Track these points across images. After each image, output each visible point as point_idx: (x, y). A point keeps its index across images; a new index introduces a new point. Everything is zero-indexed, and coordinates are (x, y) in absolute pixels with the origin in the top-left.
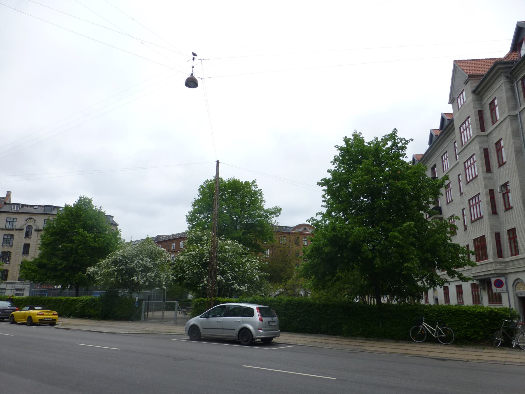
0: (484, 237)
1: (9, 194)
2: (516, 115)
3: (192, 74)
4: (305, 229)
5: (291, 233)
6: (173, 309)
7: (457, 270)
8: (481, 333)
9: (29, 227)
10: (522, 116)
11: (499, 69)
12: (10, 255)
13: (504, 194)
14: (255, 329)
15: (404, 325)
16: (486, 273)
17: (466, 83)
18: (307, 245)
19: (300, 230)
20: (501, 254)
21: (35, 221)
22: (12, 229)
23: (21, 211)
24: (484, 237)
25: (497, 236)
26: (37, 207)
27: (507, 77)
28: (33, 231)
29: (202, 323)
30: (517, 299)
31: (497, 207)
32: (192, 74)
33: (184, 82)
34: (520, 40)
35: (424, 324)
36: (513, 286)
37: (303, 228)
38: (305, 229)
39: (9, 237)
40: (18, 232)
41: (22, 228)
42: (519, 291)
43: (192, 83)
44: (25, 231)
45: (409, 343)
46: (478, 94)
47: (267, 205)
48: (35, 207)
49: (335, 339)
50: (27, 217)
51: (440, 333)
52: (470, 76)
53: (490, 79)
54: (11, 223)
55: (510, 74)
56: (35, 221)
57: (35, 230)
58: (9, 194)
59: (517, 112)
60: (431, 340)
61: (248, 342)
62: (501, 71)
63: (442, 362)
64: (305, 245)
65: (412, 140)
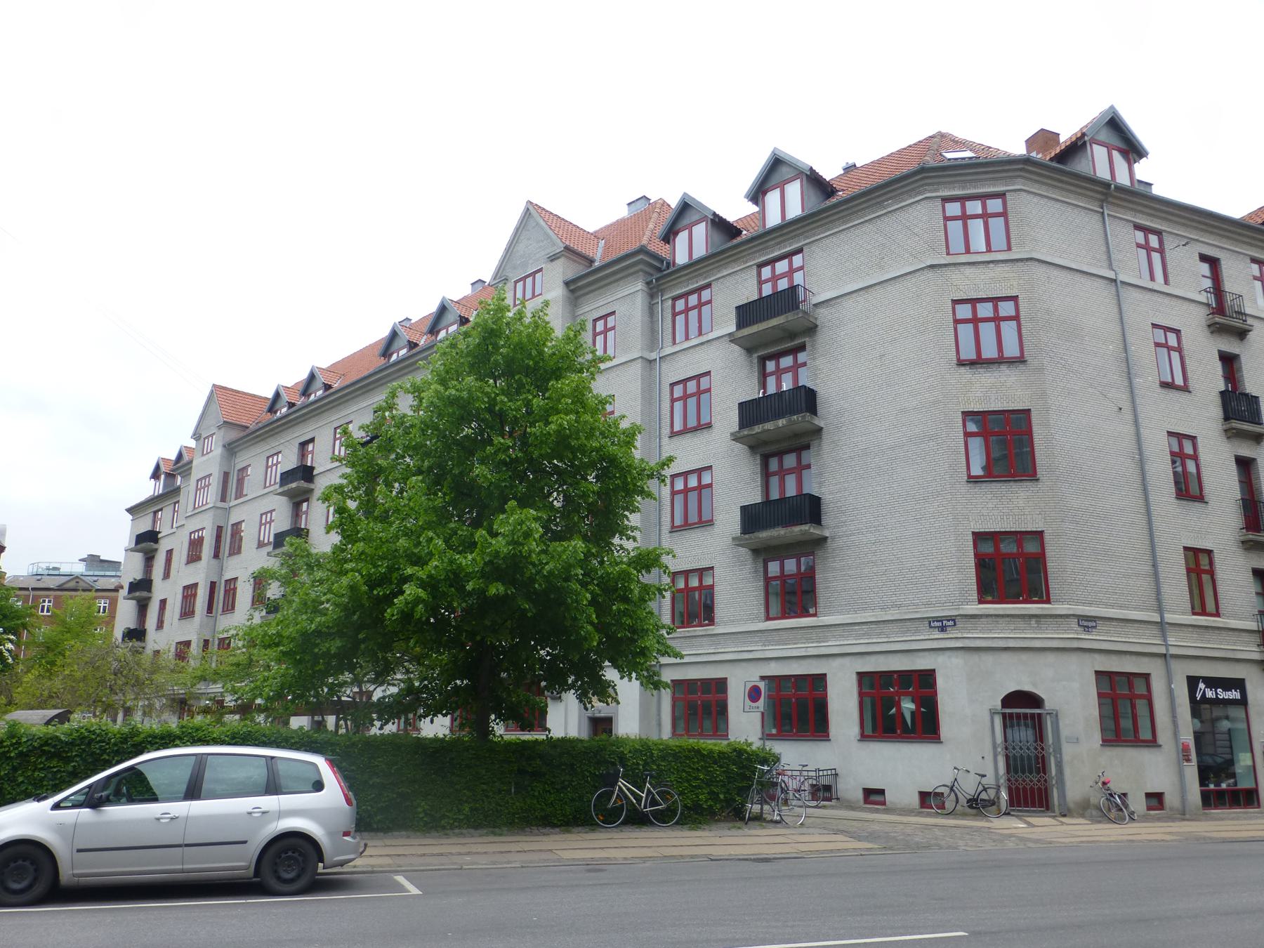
0: (196, 585)
8: (722, 796)
10: (664, 366)
11: (641, 261)
14: (331, 834)
15: (581, 791)
17: (553, 258)
24: (196, 585)
25: (213, 585)
27: (648, 283)
29: (68, 832)
34: (680, 225)
35: (621, 783)
45: (593, 830)
46: (572, 291)
49: (394, 842)
51: (654, 803)
52: (567, 248)
53: (607, 276)
54: (997, 224)
55: (657, 280)
59: (654, 356)
60: (638, 819)
61: (39, 889)
62: (641, 266)
63: (762, 866)
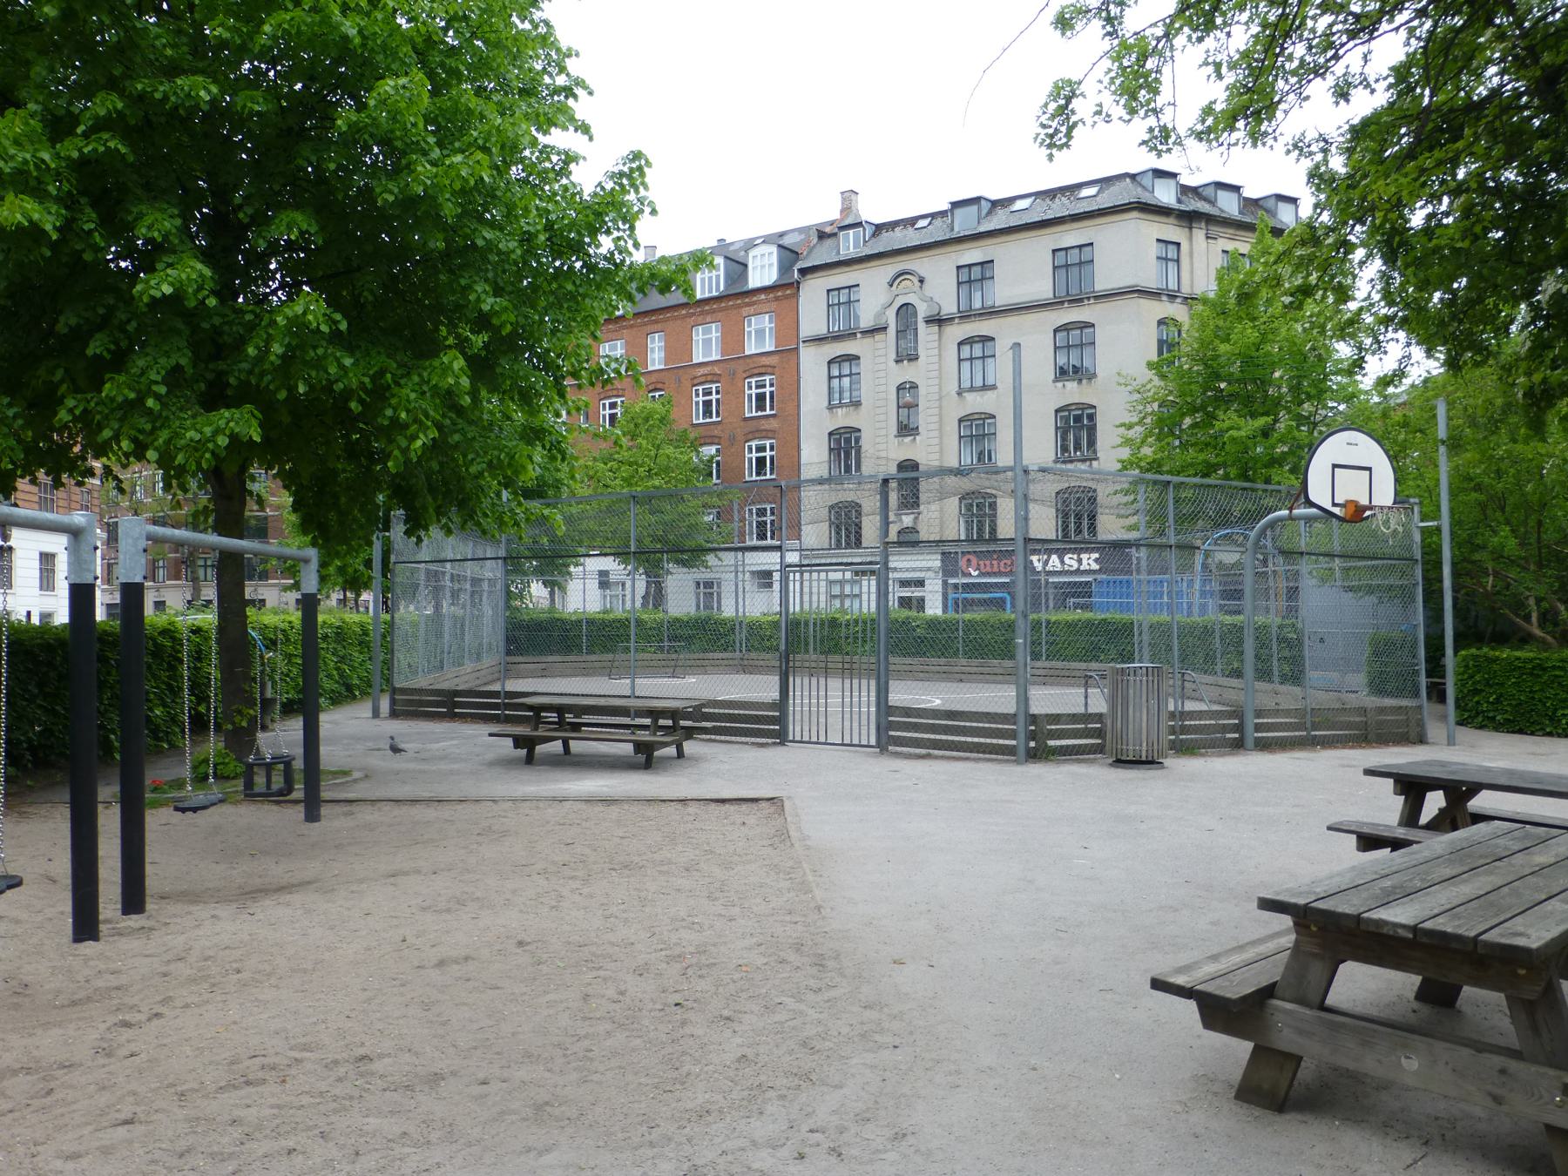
1: (849, 197)
6: (1270, 681)
7: (1353, 306)
9: (906, 310)
12: (1091, 417)
21: (921, 281)
22: (850, 335)
23: (982, 229)
26: (1092, 191)
28: (921, 326)
39: (977, 350)
40: (868, 341)
41: (882, 323)
44: (892, 330)
48: (1086, 192)
50: (890, 268)
56: (921, 281)
57: (929, 321)
58: (849, 197)
65: (591, 139)
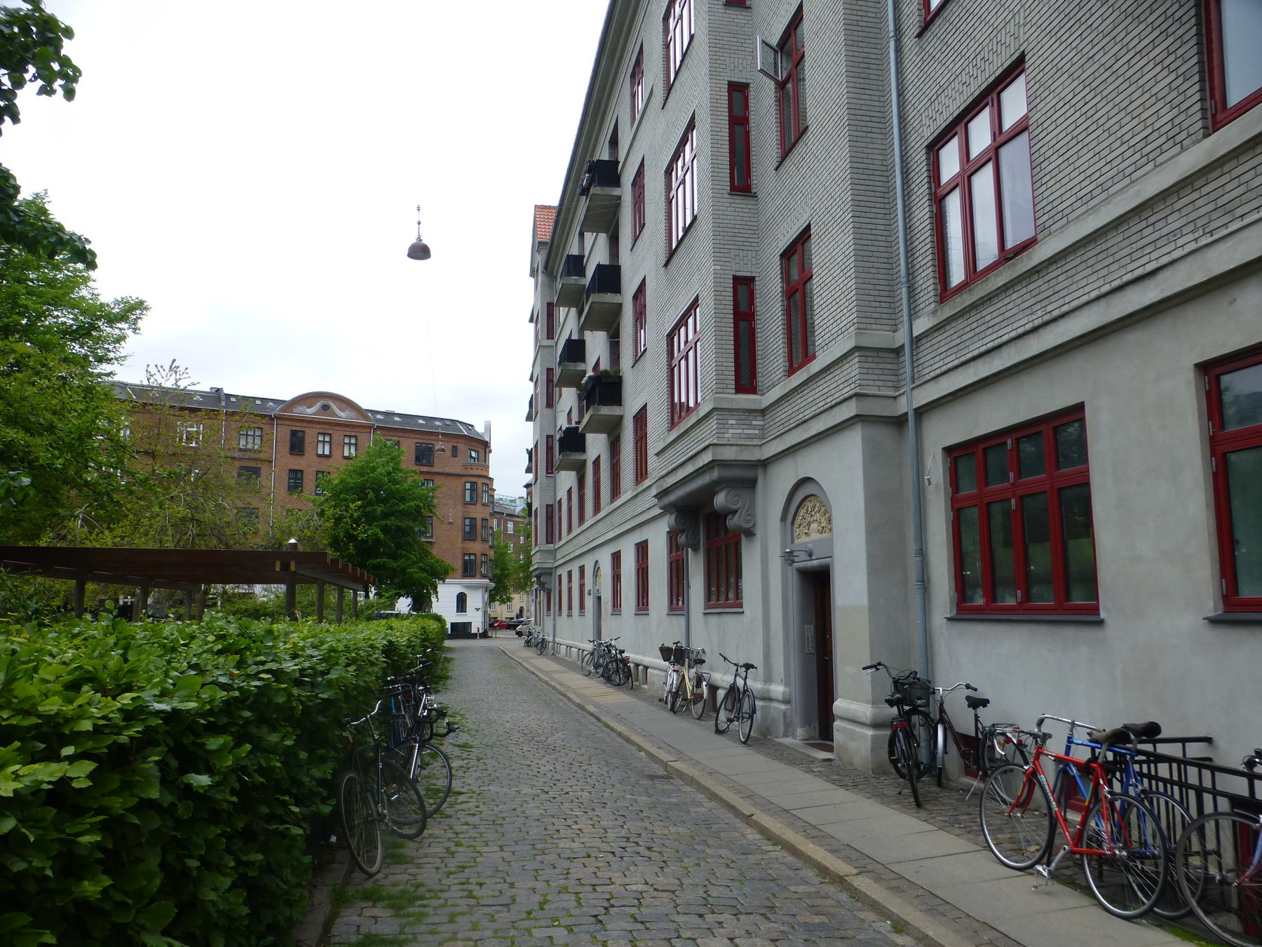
2: (898, 351)
3: (419, 239)
4: (326, 408)
5: (278, 418)
13: (781, 86)
16: (689, 469)
18: (329, 456)
19: (310, 411)
20: (753, 375)
30: (794, 579)
31: (753, 160)
32: (419, 239)
33: (406, 252)
36: (783, 519)
37: (319, 405)
38: (326, 408)
42: (804, 539)
43: (420, 251)
47: (106, 285)
59: (901, 338)
64: (323, 456)
